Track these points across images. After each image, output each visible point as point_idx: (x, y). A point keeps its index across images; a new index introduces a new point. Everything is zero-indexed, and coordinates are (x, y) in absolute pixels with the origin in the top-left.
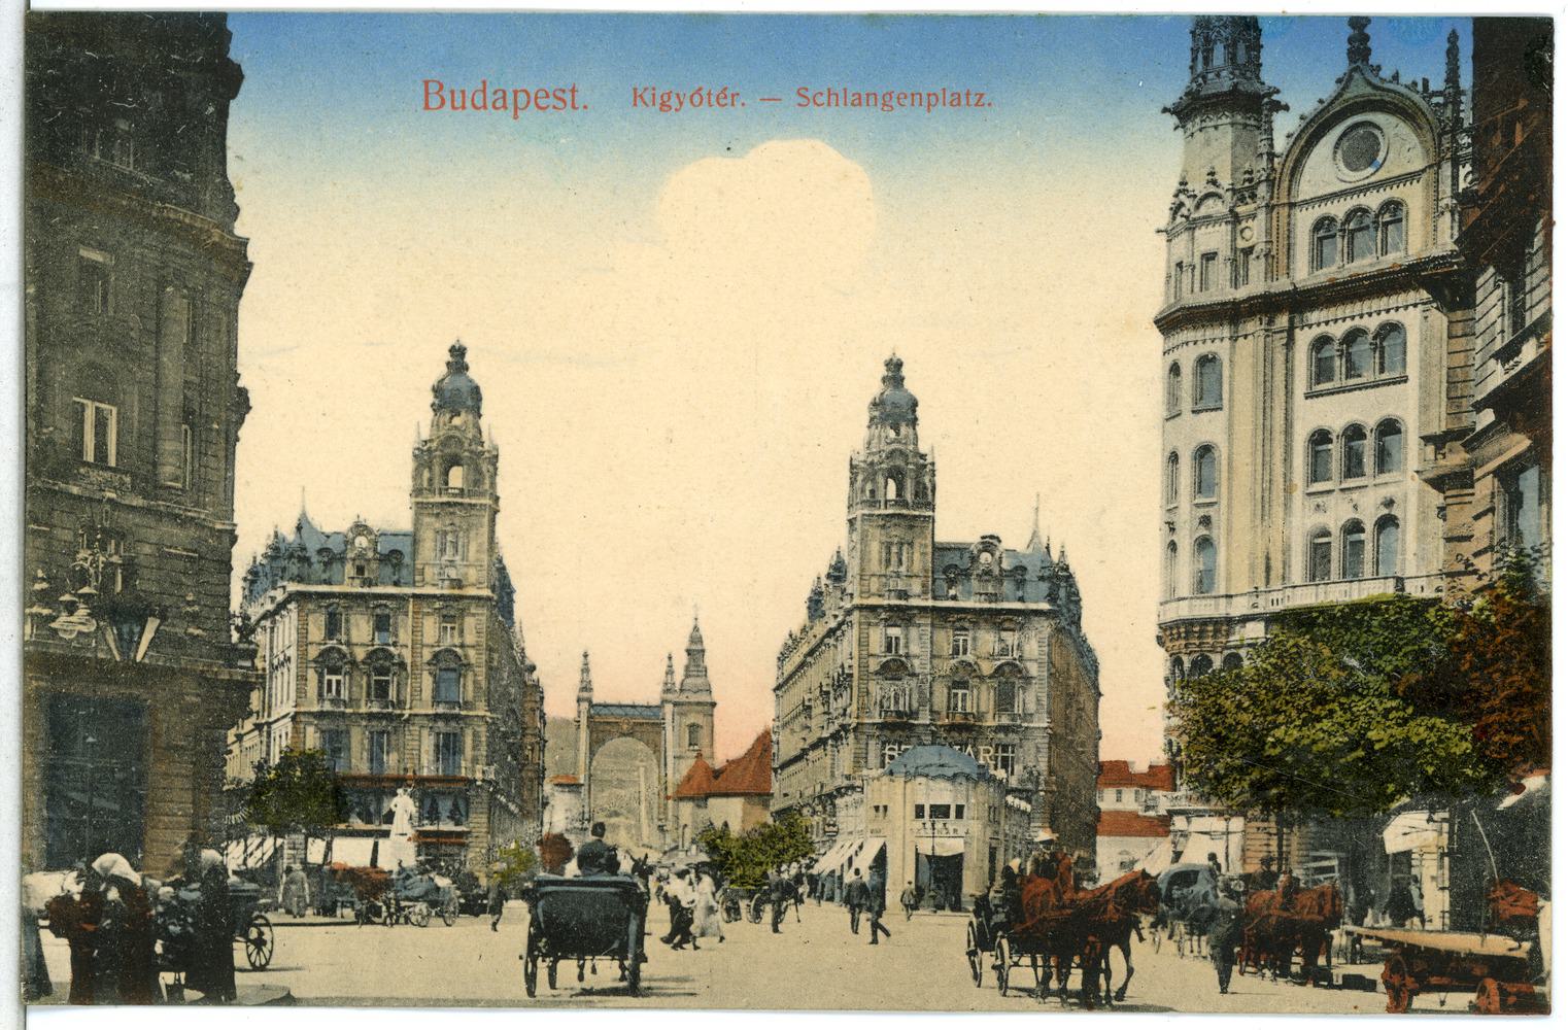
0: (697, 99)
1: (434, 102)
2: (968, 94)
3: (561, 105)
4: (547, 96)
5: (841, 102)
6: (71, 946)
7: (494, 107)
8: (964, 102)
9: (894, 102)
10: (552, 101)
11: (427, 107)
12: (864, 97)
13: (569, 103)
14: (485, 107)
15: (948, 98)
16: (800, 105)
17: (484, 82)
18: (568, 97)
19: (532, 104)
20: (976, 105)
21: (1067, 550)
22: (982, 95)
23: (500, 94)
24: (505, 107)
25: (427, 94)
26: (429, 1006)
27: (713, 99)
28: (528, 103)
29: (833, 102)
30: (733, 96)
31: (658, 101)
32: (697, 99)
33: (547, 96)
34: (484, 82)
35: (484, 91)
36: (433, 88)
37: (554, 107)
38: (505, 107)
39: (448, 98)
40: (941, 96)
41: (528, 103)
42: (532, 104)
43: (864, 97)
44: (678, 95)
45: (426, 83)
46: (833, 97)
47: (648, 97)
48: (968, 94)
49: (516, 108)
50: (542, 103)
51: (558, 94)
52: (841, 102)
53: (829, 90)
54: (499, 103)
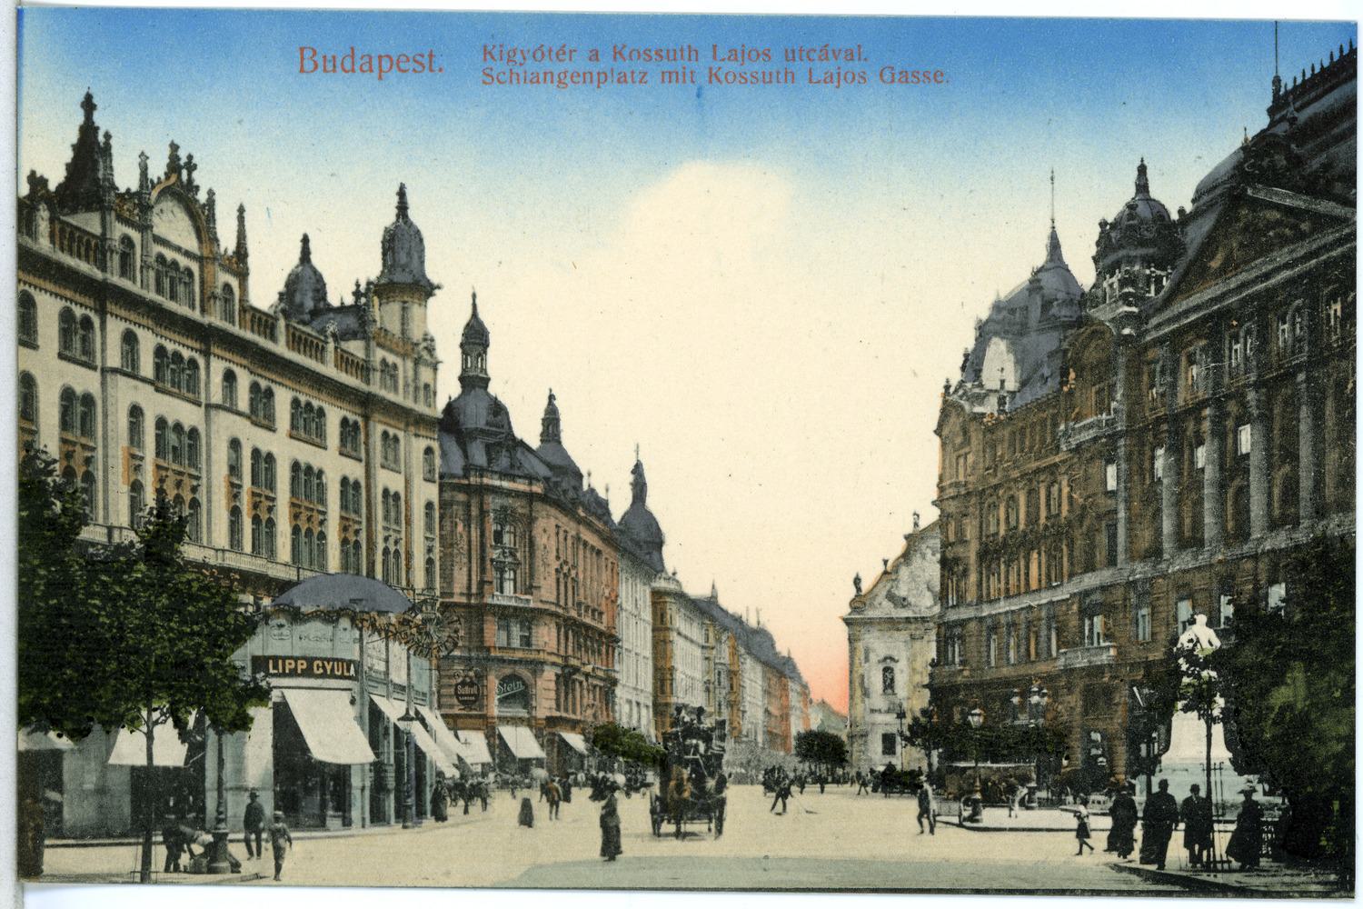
0: (539, 55)
1: (309, 65)
2: (633, 72)
3: (420, 68)
4: (408, 60)
5: (522, 81)
6: (142, 767)
7: (361, 70)
8: (629, 80)
9: (568, 80)
10: (411, 65)
11: (302, 70)
12: (541, 76)
13: (427, 66)
14: (353, 70)
15: (616, 77)
16: (484, 82)
17: (352, 49)
18: (426, 61)
19: (395, 67)
20: (641, 82)
21: (717, 586)
22: (645, 74)
23: (366, 59)
24: (371, 70)
25: (302, 59)
26: (70, 882)
27: (553, 54)
28: (391, 68)
29: (515, 81)
30: (571, 51)
31: (505, 57)
32: (539, 55)
33: (408, 60)
34: (352, 49)
35: (353, 57)
36: (308, 54)
37: (414, 70)
38: (371, 70)
39: (321, 62)
40: (609, 75)
41: (391, 68)
42: (395, 67)
43: (541, 76)
44: (522, 51)
45: (302, 50)
46: (514, 77)
47: (496, 53)
48: (801, 50)
49: (381, 71)
50: (402, 66)
51: (418, 58)
52: (522, 81)
53: (689, 46)
54: (366, 67)
